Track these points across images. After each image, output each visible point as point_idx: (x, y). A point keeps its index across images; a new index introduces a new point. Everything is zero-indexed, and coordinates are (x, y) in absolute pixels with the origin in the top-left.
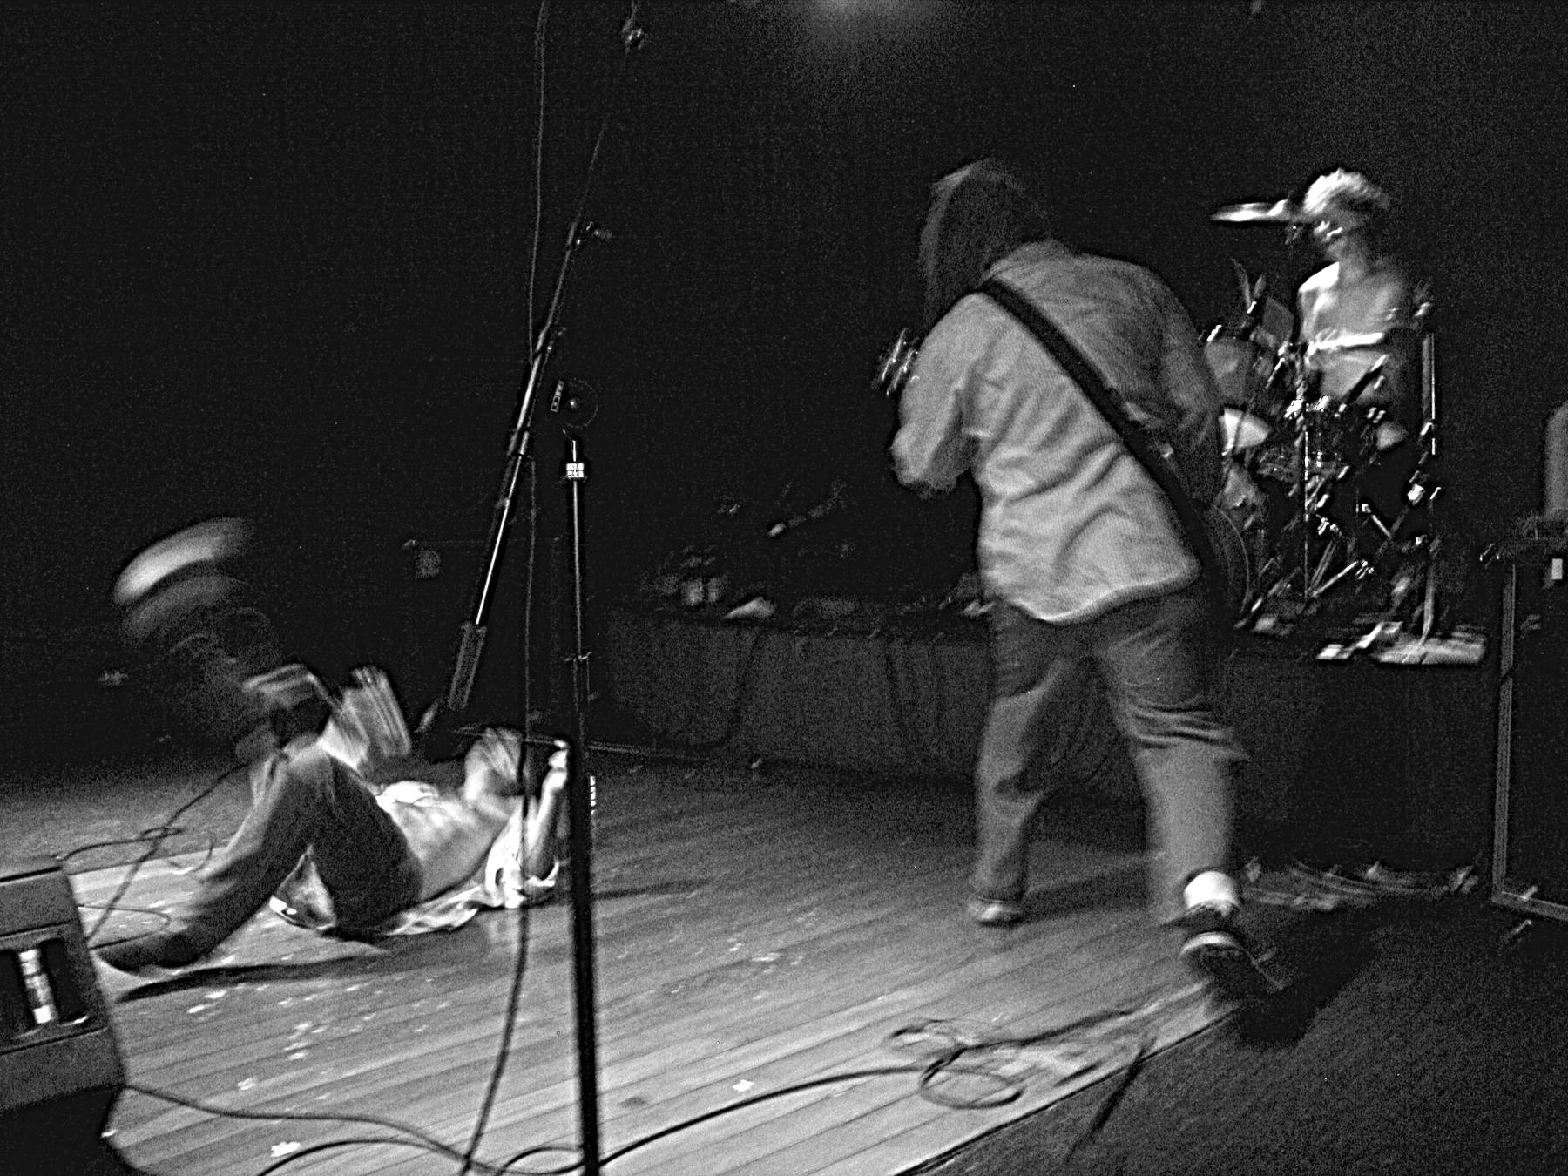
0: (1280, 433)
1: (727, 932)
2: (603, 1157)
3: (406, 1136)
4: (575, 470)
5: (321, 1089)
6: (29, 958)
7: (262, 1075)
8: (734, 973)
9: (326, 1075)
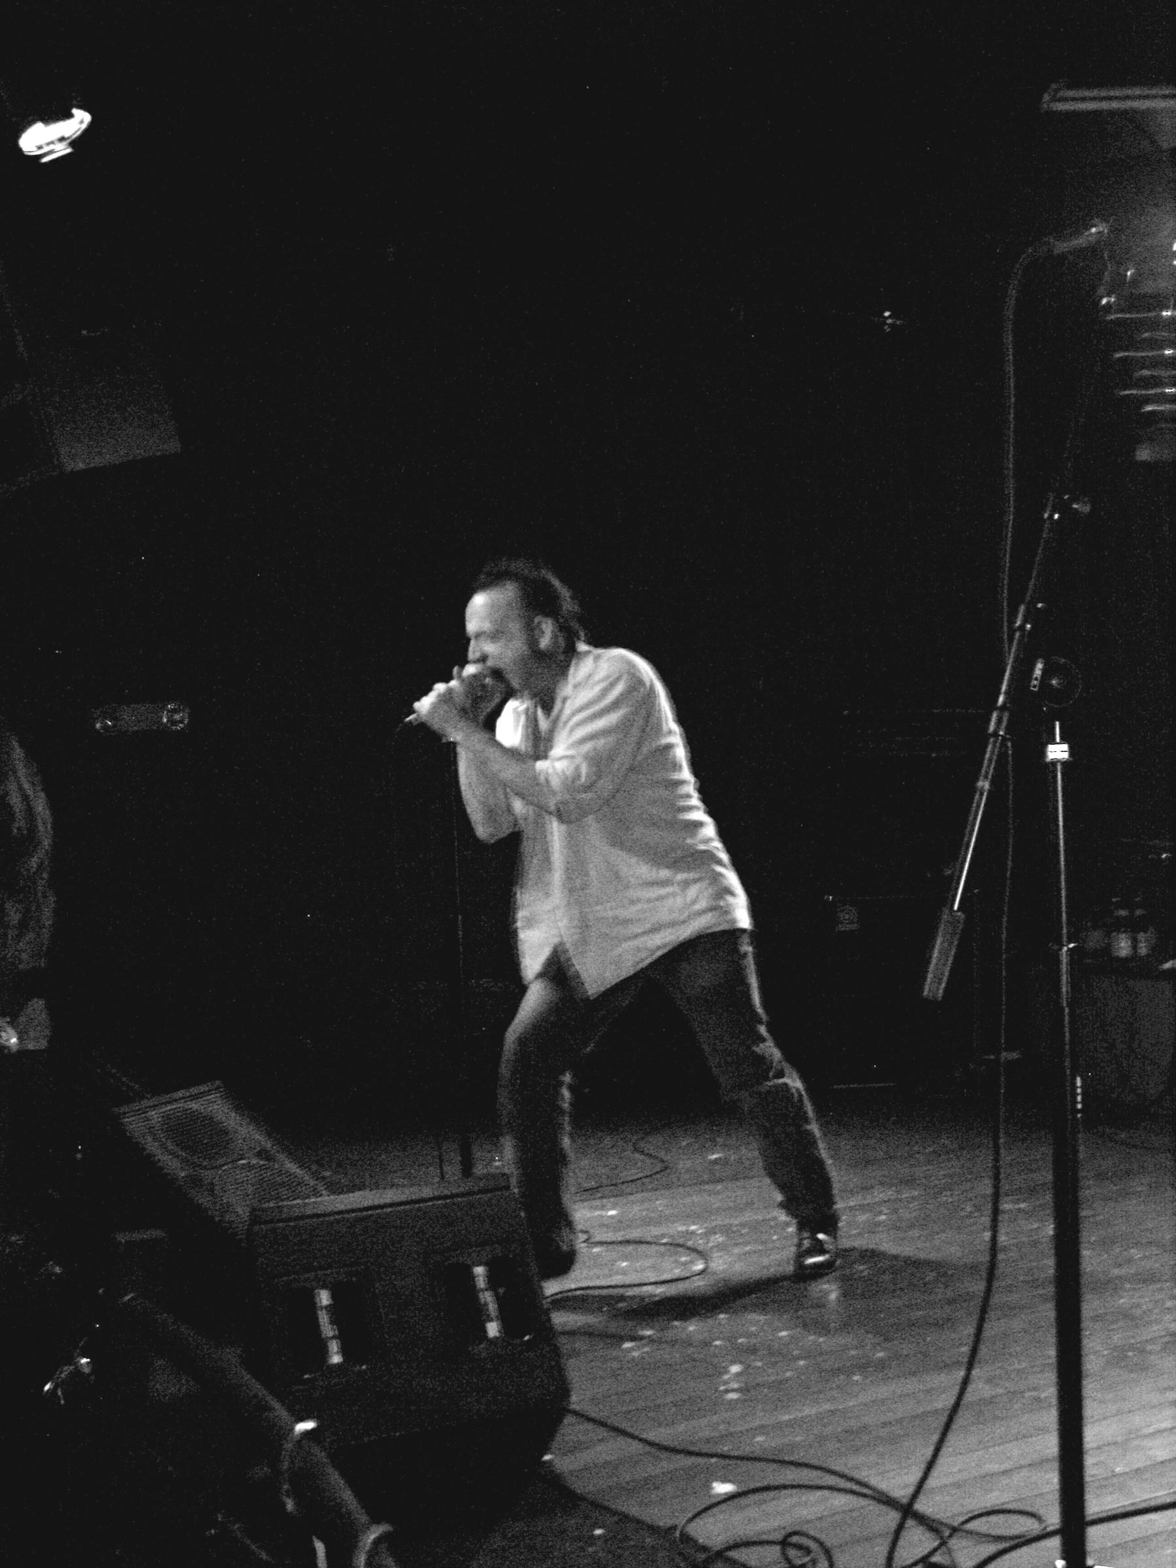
2: (1088, 1519)
4: (1058, 752)
5: (762, 1430)
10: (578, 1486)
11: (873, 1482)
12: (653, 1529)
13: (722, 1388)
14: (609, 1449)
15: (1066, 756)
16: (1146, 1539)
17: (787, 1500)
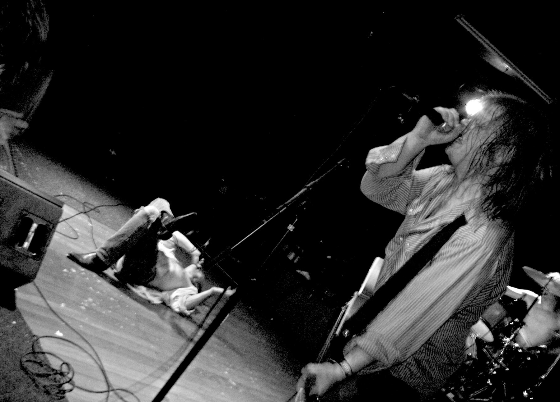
0: (497, 344)
1: (227, 366)
3: (95, 357)
4: (291, 228)
6: (35, 226)
7: (68, 305)
8: (220, 380)
9: (86, 320)
10: (19, 305)
11: (102, 361)
12: (30, 332)
13: (82, 303)
14: (37, 300)
15: (290, 225)
16: (186, 348)
17: (75, 350)
